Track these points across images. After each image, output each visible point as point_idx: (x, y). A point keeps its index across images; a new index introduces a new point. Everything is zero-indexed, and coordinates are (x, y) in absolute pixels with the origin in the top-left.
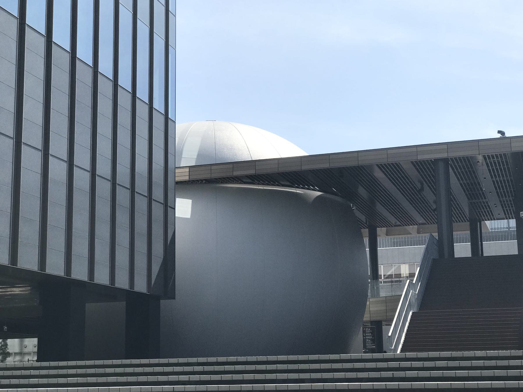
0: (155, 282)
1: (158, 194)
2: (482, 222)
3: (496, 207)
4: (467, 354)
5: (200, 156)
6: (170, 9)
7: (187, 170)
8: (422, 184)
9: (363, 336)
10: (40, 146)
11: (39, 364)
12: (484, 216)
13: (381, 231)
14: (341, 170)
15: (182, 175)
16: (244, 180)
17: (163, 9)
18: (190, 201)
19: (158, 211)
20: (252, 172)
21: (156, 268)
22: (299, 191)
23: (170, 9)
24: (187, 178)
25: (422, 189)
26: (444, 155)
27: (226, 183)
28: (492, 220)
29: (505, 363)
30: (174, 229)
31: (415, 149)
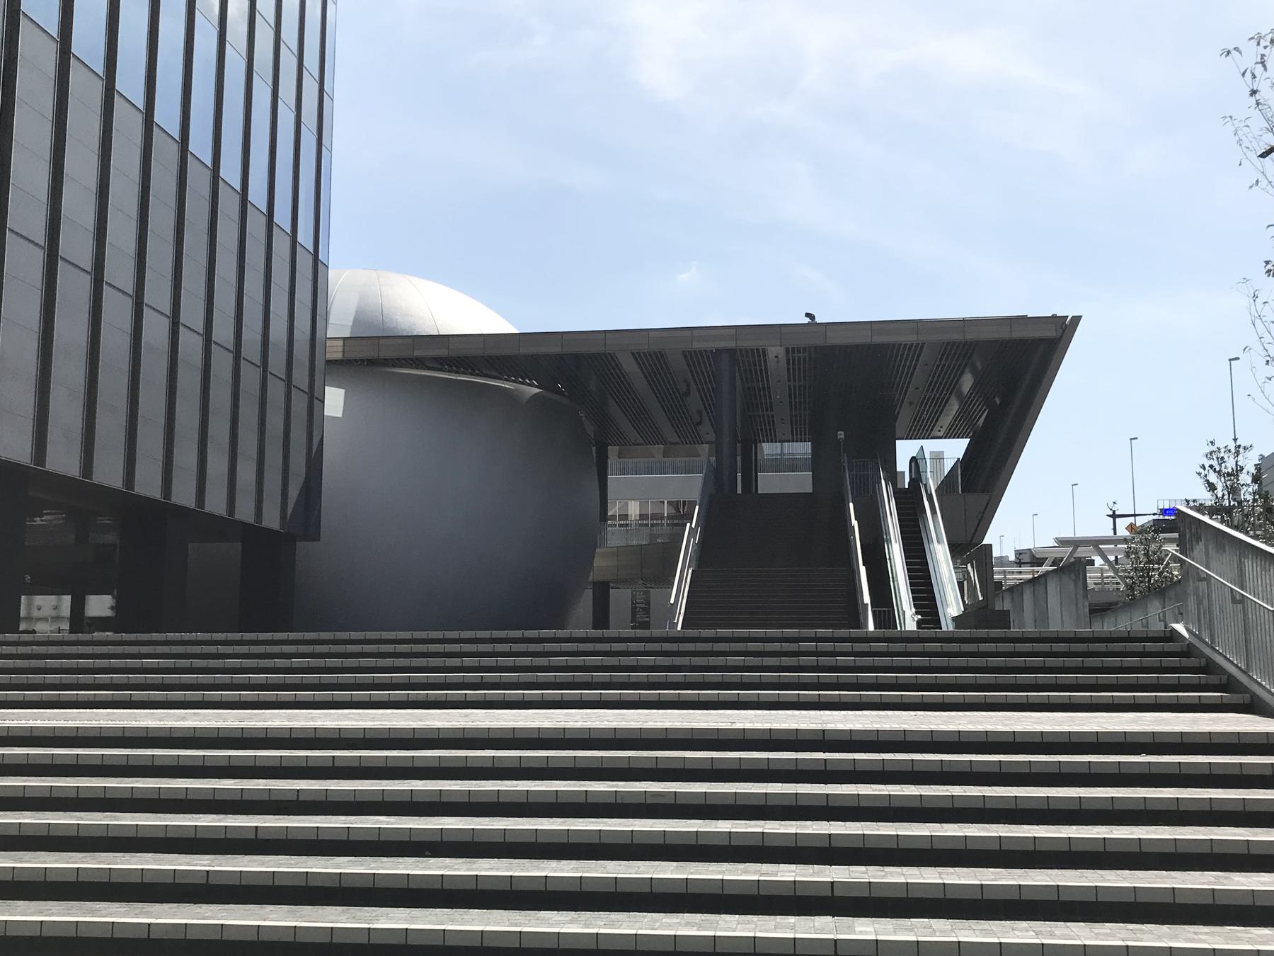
0: (291, 514)
1: (301, 378)
2: (759, 444)
3: (783, 423)
4: (386, 635)
5: (357, 322)
6: (325, 88)
7: (341, 343)
8: (688, 386)
9: (632, 603)
10: (106, 289)
11: (73, 637)
12: (763, 436)
13: (613, 451)
14: (577, 358)
15: (335, 352)
16: (428, 365)
17: (316, 87)
18: (342, 392)
19: (300, 402)
20: (443, 352)
21: (294, 492)
22: (508, 386)
23: (326, 88)
24: (339, 356)
25: (688, 393)
26: (732, 344)
27: (401, 367)
28: (772, 442)
29: (792, 647)
30: (321, 433)
31: (688, 333)
